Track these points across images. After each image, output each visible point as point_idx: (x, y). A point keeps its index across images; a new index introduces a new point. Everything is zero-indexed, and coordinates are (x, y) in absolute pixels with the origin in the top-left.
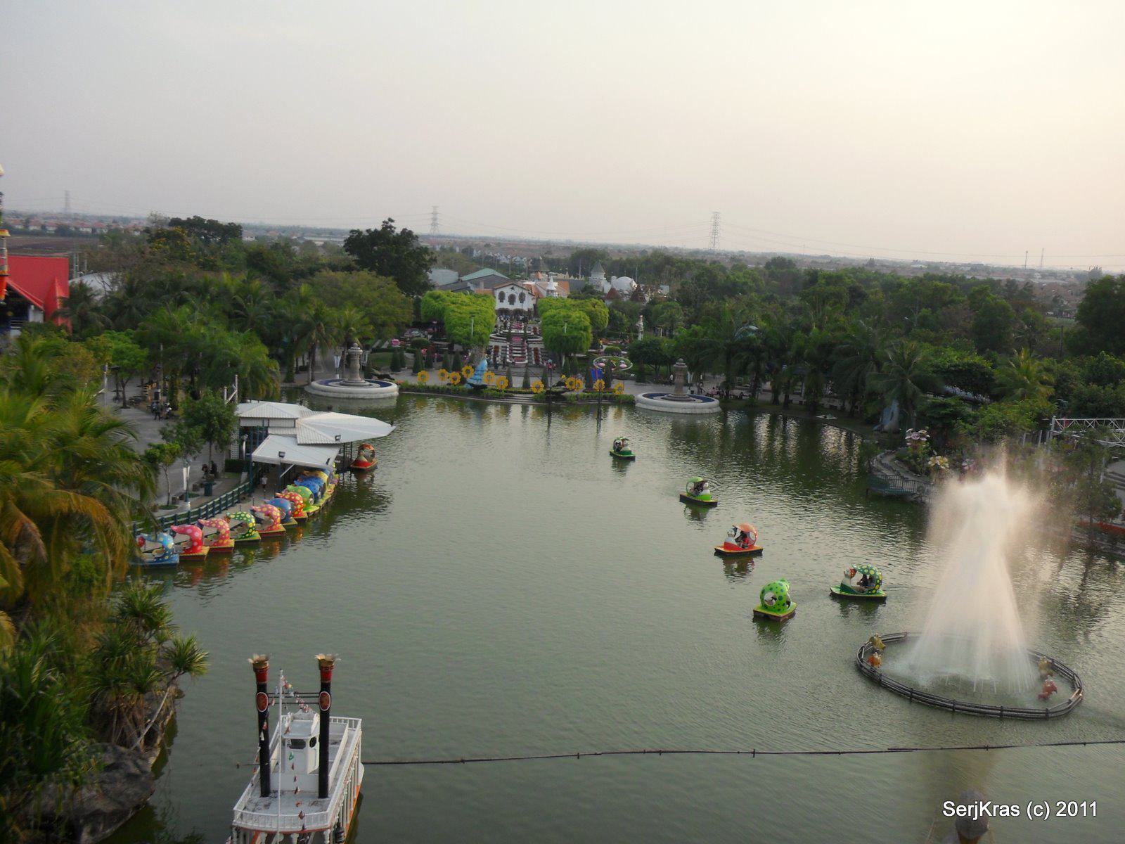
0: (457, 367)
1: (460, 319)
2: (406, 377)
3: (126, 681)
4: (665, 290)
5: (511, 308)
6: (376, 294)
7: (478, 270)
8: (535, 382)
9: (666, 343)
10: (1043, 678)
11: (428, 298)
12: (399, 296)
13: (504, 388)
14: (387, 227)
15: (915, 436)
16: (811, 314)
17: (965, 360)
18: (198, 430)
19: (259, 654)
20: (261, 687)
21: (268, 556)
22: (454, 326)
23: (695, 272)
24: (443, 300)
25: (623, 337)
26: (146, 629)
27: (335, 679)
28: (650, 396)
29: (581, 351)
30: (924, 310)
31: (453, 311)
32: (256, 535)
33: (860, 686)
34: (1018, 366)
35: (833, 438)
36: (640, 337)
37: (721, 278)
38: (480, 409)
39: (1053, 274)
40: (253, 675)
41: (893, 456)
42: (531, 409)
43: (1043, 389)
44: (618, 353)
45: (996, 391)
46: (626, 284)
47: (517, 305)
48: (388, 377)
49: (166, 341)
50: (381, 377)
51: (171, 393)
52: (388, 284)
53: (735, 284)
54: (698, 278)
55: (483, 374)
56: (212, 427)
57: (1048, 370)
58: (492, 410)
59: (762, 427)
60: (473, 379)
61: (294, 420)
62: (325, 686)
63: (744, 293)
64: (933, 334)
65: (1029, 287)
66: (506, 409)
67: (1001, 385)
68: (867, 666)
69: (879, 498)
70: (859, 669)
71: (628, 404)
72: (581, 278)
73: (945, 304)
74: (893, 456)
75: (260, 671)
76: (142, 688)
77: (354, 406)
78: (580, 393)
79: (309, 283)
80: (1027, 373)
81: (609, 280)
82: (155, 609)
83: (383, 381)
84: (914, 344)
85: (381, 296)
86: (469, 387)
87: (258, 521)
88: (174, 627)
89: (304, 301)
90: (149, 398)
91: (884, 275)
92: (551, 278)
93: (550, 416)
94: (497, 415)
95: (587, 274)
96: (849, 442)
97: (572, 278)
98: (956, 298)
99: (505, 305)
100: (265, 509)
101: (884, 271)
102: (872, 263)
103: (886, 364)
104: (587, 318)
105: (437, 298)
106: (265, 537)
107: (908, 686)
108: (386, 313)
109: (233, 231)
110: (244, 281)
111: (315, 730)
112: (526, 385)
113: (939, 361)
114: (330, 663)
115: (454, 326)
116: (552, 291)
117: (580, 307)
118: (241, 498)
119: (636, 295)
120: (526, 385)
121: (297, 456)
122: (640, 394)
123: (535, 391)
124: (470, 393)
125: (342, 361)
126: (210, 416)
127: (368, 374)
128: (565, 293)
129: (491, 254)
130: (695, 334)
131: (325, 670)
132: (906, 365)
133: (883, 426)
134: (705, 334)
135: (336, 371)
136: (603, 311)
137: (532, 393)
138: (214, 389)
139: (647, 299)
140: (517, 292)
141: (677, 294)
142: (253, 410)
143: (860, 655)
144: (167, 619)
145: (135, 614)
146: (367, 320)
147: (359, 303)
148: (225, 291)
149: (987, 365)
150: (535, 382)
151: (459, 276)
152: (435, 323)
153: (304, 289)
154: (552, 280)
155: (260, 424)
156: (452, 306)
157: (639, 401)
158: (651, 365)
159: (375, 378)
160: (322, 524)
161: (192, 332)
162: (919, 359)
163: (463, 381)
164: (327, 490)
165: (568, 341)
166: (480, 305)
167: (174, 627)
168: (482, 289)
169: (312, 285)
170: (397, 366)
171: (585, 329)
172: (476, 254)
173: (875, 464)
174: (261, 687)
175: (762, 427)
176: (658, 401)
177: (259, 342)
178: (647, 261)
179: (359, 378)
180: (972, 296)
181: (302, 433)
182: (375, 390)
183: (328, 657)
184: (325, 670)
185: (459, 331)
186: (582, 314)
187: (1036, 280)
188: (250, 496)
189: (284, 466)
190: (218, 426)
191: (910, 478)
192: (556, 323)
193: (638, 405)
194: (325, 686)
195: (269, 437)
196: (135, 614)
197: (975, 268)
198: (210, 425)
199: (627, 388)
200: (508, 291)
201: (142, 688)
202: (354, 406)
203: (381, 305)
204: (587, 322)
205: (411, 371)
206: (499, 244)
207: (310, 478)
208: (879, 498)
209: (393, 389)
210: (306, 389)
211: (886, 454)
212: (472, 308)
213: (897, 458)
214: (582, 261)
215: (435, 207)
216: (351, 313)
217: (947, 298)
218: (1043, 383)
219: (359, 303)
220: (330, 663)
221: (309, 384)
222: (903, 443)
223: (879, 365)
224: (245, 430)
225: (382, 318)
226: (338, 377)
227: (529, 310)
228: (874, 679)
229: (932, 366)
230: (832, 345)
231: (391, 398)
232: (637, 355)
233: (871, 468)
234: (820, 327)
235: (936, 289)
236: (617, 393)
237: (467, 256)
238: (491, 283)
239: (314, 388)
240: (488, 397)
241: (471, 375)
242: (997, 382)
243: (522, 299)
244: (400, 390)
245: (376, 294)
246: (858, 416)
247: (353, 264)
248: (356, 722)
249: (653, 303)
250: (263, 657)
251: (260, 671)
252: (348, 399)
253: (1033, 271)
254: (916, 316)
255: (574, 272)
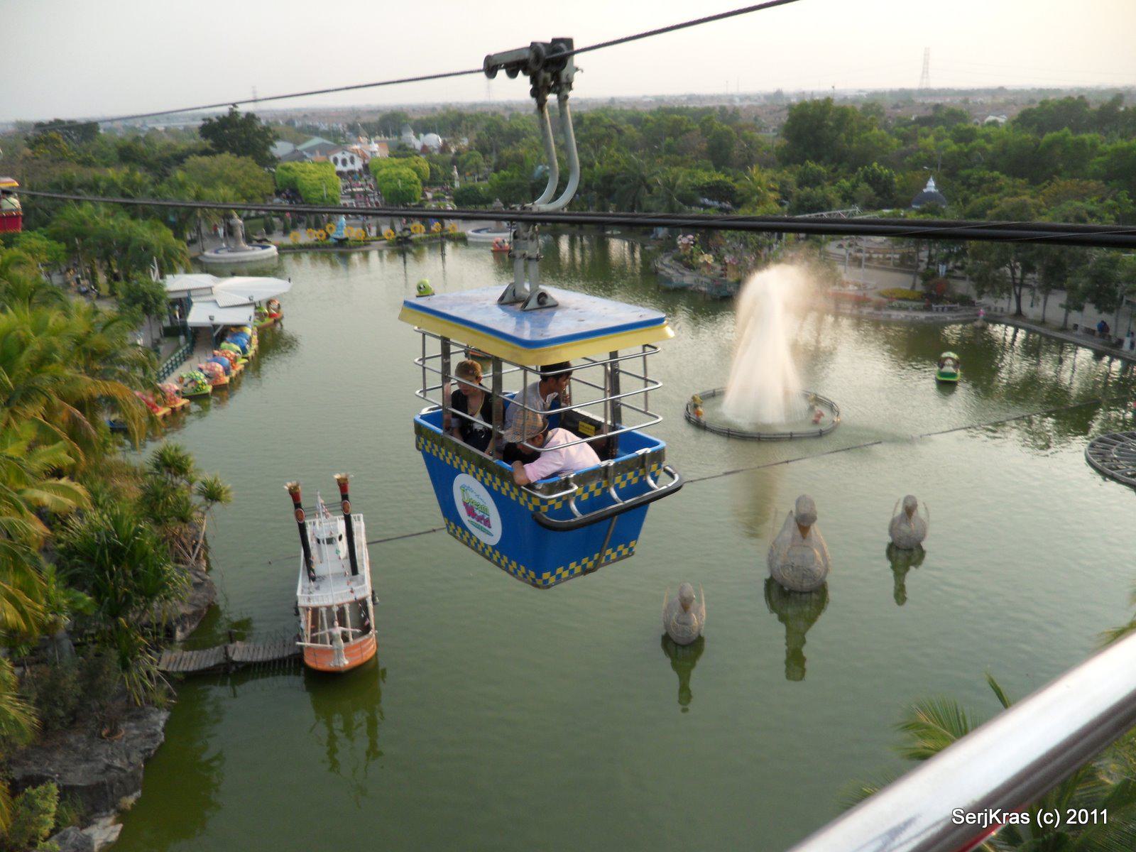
0: (318, 226)
1: (312, 185)
2: (278, 238)
3: (171, 516)
4: (465, 142)
5: (345, 169)
6: (241, 172)
7: (310, 139)
8: (386, 230)
9: (483, 186)
10: (812, 408)
11: (281, 170)
12: (261, 172)
13: (362, 239)
14: (233, 114)
15: (685, 240)
16: (592, 152)
17: (714, 179)
18: (138, 308)
19: (291, 481)
20: (298, 506)
21: (222, 401)
22: (309, 192)
23: (484, 124)
24: (293, 171)
25: (442, 185)
26: (176, 475)
27: (350, 493)
28: (478, 231)
29: (415, 200)
30: (668, 139)
31: (305, 179)
32: (209, 389)
33: (690, 431)
34: (752, 179)
35: (618, 247)
36: (457, 184)
37: (505, 127)
38: (345, 257)
39: (747, 97)
40: (290, 499)
41: (670, 257)
42: (386, 253)
43: (772, 195)
44: (443, 199)
45: (738, 199)
46: (434, 140)
47: (350, 167)
48: (266, 240)
49: (82, 236)
50: (260, 241)
51: (93, 277)
52: (248, 162)
53: (517, 130)
54: (488, 129)
55: (344, 228)
56: (146, 303)
57: (773, 180)
58: (355, 257)
59: (564, 244)
60: (335, 234)
61: (211, 288)
62: (345, 497)
63: (526, 137)
64: (679, 158)
65: (736, 112)
66: (366, 254)
67: (741, 195)
68: (693, 417)
69: (667, 291)
70: (688, 419)
71: (461, 240)
72: (396, 138)
73: (682, 133)
74: (670, 257)
75: (294, 494)
76: (184, 520)
77: (244, 268)
78: (423, 235)
79: (182, 169)
80: (760, 184)
81: (418, 137)
82: (181, 459)
83: (263, 244)
84: (675, 170)
85: (246, 173)
86: (334, 241)
87: (207, 376)
88: (198, 471)
89: (182, 185)
90: (73, 284)
91: (627, 111)
92: (372, 140)
93: (404, 257)
94: (360, 261)
95: (399, 134)
96: (632, 250)
97: (387, 138)
98: (689, 127)
99: (340, 167)
100: (209, 367)
101: (625, 108)
102: (612, 101)
103: (655, 188)
104: (414, 173)
105: (288, 169)
106: (215, 388)
107: (726, 427)
108: (253, 188)
109: (88, 129)
110: (127, 174)
111: (341, 527)
112: (379, 234)
113: (694, 181)
114: (346, 479)
115: (309, 192)
116: (375, 152)
117: (407, 164)
118: (186, 357)
119: (444, 149)
120: (379, 234)
121: (224, 318)
122: (469, 229)
123: (387, 237)
124: (336, 245)
125: (224, 233)
126: (145, 295)
127: (249, 240)
128: (386, 153)
129: (311, 124)
130: (504, 178)
131: (343, 486)
132: (670, 186)
133: (657, 235)
134: (512, 177)
135: (222, 241)
136: (425, 166)
137: (385, 239)
138: (144, 272)
139: (453, 150)
140: (347, 156)
141: (474, 144)
142: (177, 283)
143: (687, 409)
144: (192, 465)
145: (168, 465)
146: (239, 195)
147: (229, 181)
148: (112, 185)
149: (729, 180)
150: (386, 230)
151: (295, 147)
152: (292, 191)
153: (179, 175)
154: (373, 142)
155: (185, 295)
156: (303, 175)
157: (469, 236)
158: (471, 205)
159: (255, 243)
160: (254, 366)
161: (102, 224)
162: (679, 182)
163: (328, 236)
164: (253, 340)
165: (403, 193)
166: (320, 172)
167: (198, 471)
168: (318, 157)
169: (185, 170)
170: (269, 230)
171: (416, 183)
172: (297, 124)
173: (659, 266)
174: (298, 506)
175: (564, 244)
176: (484, 234)
177: (164, 227)
178: (444, 118)
179: (243, 244)
180: (702, 125)
181: (218, 298)
182: (257, 253)
183: (343, 475)
184: (343, 486)
185: (314, 195)
186: (410, 171)
187: (737, 103)
188: (192, 354)
189: (215, 327)
190: (153, 303)
191: (686, 273)
192: (390, 180)
193: (469, 239)
194: (345, 497)
195: (194, 304)
196: (168, 465)
197: (691, 98)
198: (147, 302)
199: (455, 227)
200: (340, 156)
201: (184, 520)
202: (244, 268)
203: (247, 181)
204: (415, 177)
205: (282, 233)
206: (314, 114)
207: (237, 334)
208: (667, 291)
209: (273, 250)
210: (201, 258)
211: (666, 256)
212: (319, 175)
213: (674, 259)
214: (389, 123)
215: (253, 87)
216: (225, 192)
217: (683, 128)
218: (773, 190)
219: (229, 181)
220: (346, 479)
221: (202, 254)
222: (675, 246)
223: (650, 190)
224: (174, 303)
225: (250, 192)
226: (224, 245)
227: (360, 170)
228: (699, 425)
229: (690, 185)
230: (612, 176)
231: (273, 257)
232: (460, 198)
233: (656, 269)
234: (601, 163)
235: (675, 121)
236: (451, 232)
237: (300, 128)
238: (325, 150)
239: (208, 258)
240: (350, 247)
241: (334, 231)
242: (739, 193)
243: (352, 160)
244: (279, 250)
245: (241, 172)
246: (633, 229)
247: (210, 148)
248: (359, 517)
249: (458, 153)
250: (294, 483)
251: (294, 494)
252: (238, 263)
253: (732, 96)
254: (663, 144)
255: (387, 134)
